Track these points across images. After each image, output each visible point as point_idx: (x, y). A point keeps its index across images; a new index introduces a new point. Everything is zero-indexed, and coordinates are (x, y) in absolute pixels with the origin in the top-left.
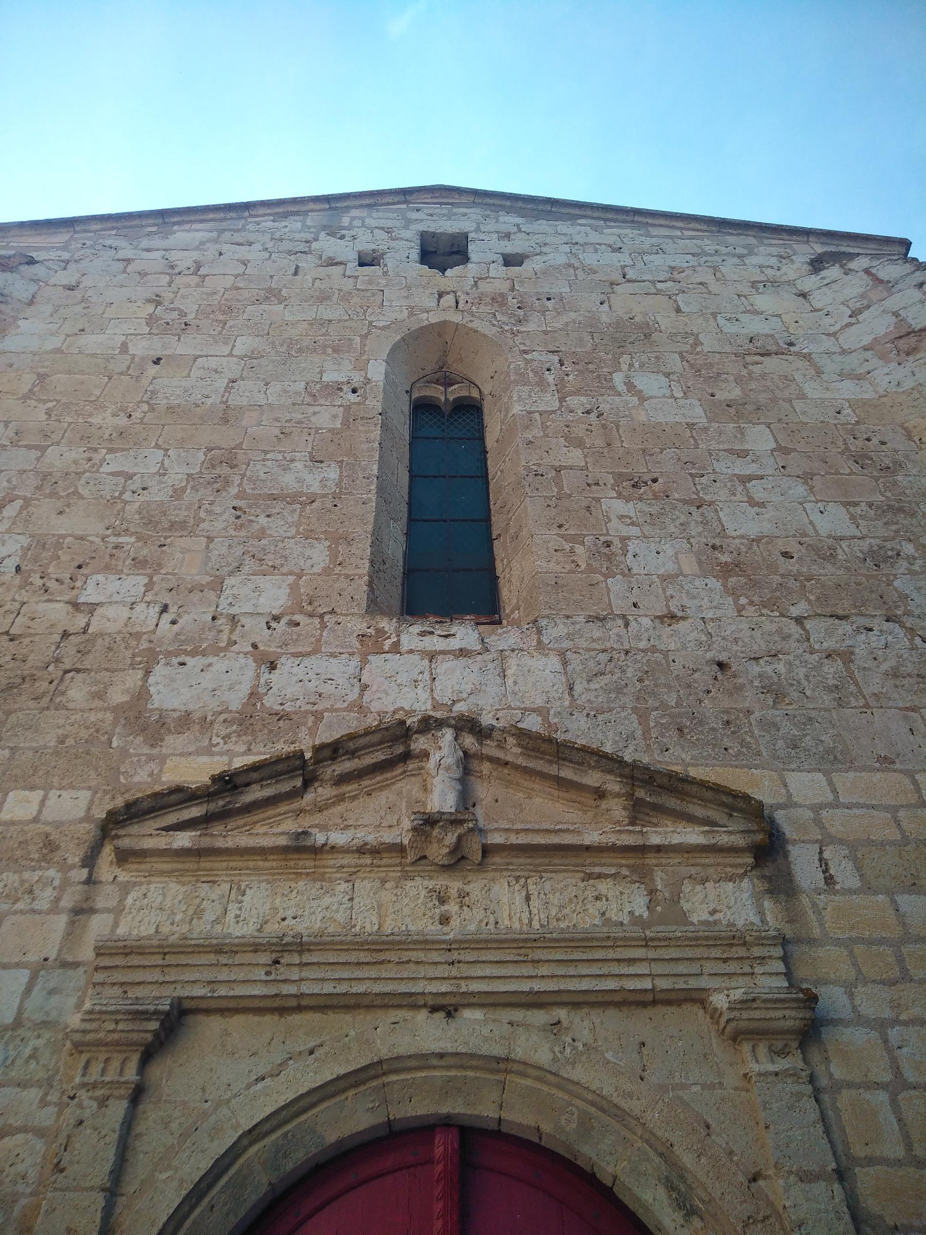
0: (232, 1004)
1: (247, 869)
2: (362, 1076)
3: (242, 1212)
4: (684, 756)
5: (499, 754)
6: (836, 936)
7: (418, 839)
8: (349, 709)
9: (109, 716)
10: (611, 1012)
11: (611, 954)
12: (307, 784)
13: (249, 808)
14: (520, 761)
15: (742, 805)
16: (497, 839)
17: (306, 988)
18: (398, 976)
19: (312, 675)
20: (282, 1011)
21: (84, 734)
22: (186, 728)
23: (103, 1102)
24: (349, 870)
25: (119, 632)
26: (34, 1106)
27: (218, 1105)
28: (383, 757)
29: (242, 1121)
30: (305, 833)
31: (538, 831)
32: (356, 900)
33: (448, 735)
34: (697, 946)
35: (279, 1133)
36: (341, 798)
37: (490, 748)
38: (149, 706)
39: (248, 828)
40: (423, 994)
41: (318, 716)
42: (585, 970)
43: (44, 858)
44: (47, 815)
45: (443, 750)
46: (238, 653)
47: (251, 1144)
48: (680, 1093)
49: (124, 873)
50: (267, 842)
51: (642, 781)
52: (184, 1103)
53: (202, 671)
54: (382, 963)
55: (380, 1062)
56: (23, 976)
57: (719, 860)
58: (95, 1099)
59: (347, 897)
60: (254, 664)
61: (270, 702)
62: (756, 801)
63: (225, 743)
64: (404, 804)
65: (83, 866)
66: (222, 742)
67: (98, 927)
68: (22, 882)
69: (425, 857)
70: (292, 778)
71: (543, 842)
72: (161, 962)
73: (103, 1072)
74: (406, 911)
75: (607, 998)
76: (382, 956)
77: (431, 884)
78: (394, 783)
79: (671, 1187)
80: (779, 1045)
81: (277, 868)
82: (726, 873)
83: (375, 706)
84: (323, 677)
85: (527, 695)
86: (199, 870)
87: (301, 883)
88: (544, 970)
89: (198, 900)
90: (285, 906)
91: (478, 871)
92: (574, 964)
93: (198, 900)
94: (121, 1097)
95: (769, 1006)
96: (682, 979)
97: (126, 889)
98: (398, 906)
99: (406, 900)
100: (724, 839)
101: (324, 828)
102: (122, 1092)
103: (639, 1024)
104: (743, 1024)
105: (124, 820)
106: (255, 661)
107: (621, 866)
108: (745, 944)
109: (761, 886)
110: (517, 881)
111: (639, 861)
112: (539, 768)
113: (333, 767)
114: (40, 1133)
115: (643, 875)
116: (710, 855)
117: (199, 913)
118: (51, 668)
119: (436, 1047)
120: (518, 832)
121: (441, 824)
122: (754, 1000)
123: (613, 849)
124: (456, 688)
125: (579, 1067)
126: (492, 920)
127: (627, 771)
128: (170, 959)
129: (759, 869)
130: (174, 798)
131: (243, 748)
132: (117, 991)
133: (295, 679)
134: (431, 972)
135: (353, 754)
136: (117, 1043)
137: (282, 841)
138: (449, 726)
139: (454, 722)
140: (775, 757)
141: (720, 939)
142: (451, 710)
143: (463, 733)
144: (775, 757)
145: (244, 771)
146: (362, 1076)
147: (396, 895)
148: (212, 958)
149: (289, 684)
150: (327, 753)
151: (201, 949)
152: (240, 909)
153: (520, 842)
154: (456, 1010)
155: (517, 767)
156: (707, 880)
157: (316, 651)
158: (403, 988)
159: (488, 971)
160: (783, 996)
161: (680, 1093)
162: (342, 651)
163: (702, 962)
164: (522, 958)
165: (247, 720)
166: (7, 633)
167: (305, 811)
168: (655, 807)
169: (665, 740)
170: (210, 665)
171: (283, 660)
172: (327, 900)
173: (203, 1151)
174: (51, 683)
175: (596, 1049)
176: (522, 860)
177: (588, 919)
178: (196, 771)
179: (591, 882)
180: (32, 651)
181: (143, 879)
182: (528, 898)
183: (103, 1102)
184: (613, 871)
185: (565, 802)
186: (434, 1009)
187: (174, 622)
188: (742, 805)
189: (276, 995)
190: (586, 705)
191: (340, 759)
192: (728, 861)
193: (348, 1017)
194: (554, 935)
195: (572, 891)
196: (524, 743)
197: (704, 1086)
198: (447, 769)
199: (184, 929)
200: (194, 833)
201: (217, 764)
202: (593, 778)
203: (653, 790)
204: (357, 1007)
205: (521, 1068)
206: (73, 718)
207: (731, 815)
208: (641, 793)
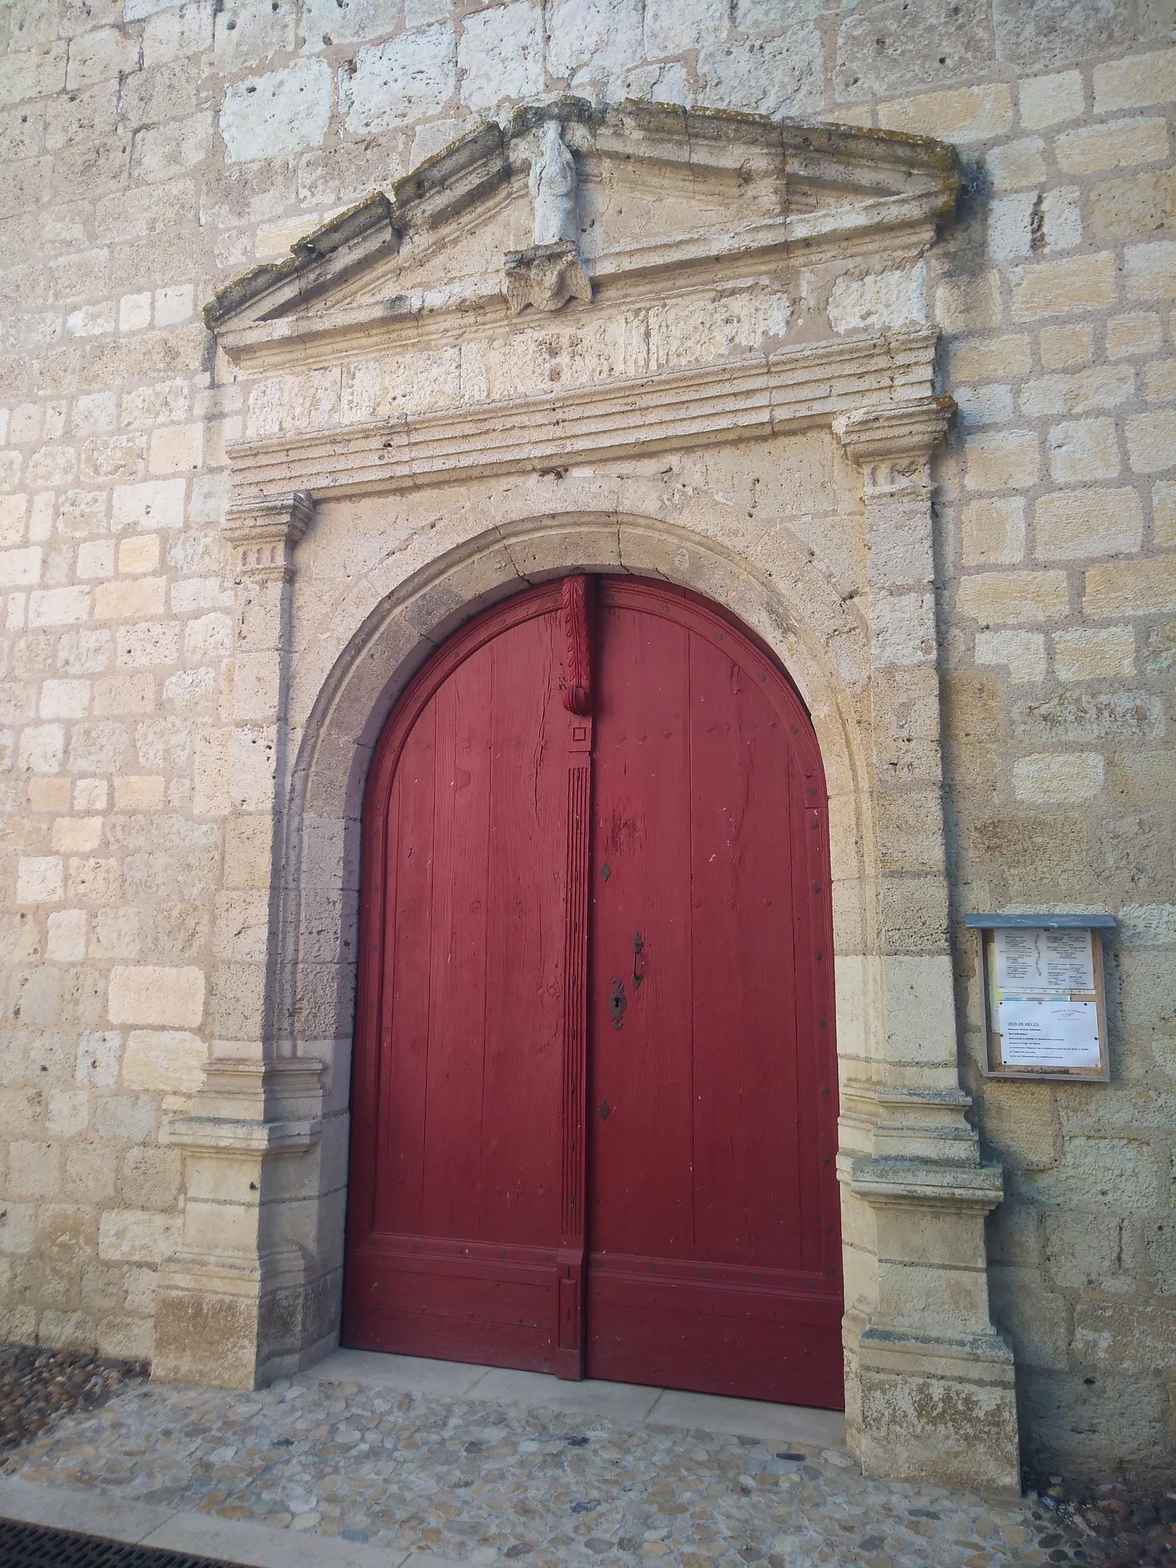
0: (355, 490)
1: (353, 349)
2: (482, 542)
3: (402, 658)
4: (876, 86)
5: (615, 145)
6: (1023, 320)
7: (517, 284)
8: (444, 115)
9: (190, 184)
10: (727, 451)
11: (727, 388)
12: (400, 233)
13: (344, 276)
14: (645, 151)
15: (923, 156)
16: (606, 268)
17: (417, 468)
18: (504, 444)
19: (398, 72)
20: (401, 491)
21: (171, 213)
22: (268, 182)
23: (263, 584)
24: (454, 333)
25: (177, 58)
26: (217, 591)
27: (359, 578)
28: (478, 181)
29: (380, 590)
30: (400, 298)
31: (655, 248)
32: (464, 367)
33: (551, 129)
34: (830, 363)
35: (417, 596)
36: (441, 245)
37: (606, 141)
38: (228, 161)
39: (348, 300)
40: (529, 459)
41: (408, 132)
42: (695, 411)
43: (169, 367)
44: (162, 320)
45: (543, 153)
46: (309, 57)
47: (393, 607)
48: (788, 525)
49: (242, 372)
50: (362, 316)
51: (795, 147)
52: (331, 579)
53: (274, 95)
54: (487, 432)
55: (496, 528)
56: (181, 484)
57: (887, 243)
58: (257, 582)
59: (455, 365)
60: (330, 70)
61: (354, 125)
62: (944, 147)
63: (313, 195)
64: (512, 238)
65: (205, 370)
66: (309, 194)
67: (230, 430)
68: (157, 394)
69: (530, 305)
70: (379, 230)
71: (660, 261)
72: (285, 459)
73: (258, 561)
74: (515, 371)
75: (720, 438)
76: (486, 426)
77: (540, 335)
78: (499, 212)
79: (771, 611)
80: (904, 463)
81: (381, 343)
82: (893, 260)
83: (476, 103)
84: (411, 70)
85: (672, 34)
86: (307, 358)
87: (408, 356)
88: (653, 417)
89: (313, 390)
90: (394, 384)
91: (592, 310)
92: (686, 405)
93: (313, 390)
94: (276, 580)
95: (894, 423)
96: (807, 405)
97: (246, 387)
98: (506, 367)
99: (514, 359)
100: (893, 212)
101: (426, 286)
102: (276, 575)
103: (756, 460)
104: (861, 448)
105: (222, 316)
106: (330, 66)
107: (760, 274)
108: (888, 352)
109: (938, 267)
110: (637, 315)
111: (782, 264)
112: (666, 156)
113: (423, 207)
114: (226, 611)
115: (786, 281)
116: (876, 238)
117: (315, 403)
118: (120, 131)
119: (547, 509)
120: (631, 253)
121: (536, 263)
122: (876, 419)
123: (748, 254)
124: (577, 46)
125: (686, 511)
126: (606, 368)
127: (774, 136)
128: (293, 455)
129: (942, 245)
130: (261, 281)
131: (332, 198)
132: (254, 490)
133: (380, 81)
134: (536, 435)
135: (442, 184)
136: (261, 536)
137: (378, 312)
138: (552, 118)
139: (557, 111)
140: (1014, 58)
141: (857, 351)
142: (569, 86)
143: (572, 124)
144: (1014, 58)
145: (323, 234)
146: (482, 542)
147: (504, 354)
148: (329, 449)
149: (373, 93)
150: (409, 190)
151: (318, 442)
152: (352, 394)
153: (633, 267)
154: (566, 470)
155: (641, 160)
156: (867, 273)
157: (399, 29)
158: (509, 456)
159: (594, 426)
160: (910, 410)
161: (788, 525)
162: (431, 20)
163: (832, 382)
164: (629, 408)
165: (328, 161)
166: (64, 90)
167: (406, 269)
168: (815, 183)
169: (854, 66)
170: (281, 84)
171: (362, 55)
172: (435, 371)
173: (352, 616)
174: (124, 152)
175: (706, 492)
176: (641, 289)
177: (712, 350)
178: (275, 244)
179: (724, 300)
180: (95, 111)
181: (261, 376)
182: (647, 334)
183: (263, 584)
184: (749, 282)
185: (703, 197)
186: (544, 472)
187: (232, 26)
188: (923, 156)
189: (392, 477)
190: (751, 32)
191: (428, 195)
192: (898, 242)
193: (463, 490)
194: (663, 377)
195: (699, 316)
196: (645, 123)
197: (815, 515)
198: (551, 182)
199: (304, 422)
200: (290, 319)
201: (306, 226)
202: (732, 157)
203: (811, 155)
204: (469, 479)
205: (631, 518)
206: (155, 194)
207: (910, 175)
208: (794, 166)
